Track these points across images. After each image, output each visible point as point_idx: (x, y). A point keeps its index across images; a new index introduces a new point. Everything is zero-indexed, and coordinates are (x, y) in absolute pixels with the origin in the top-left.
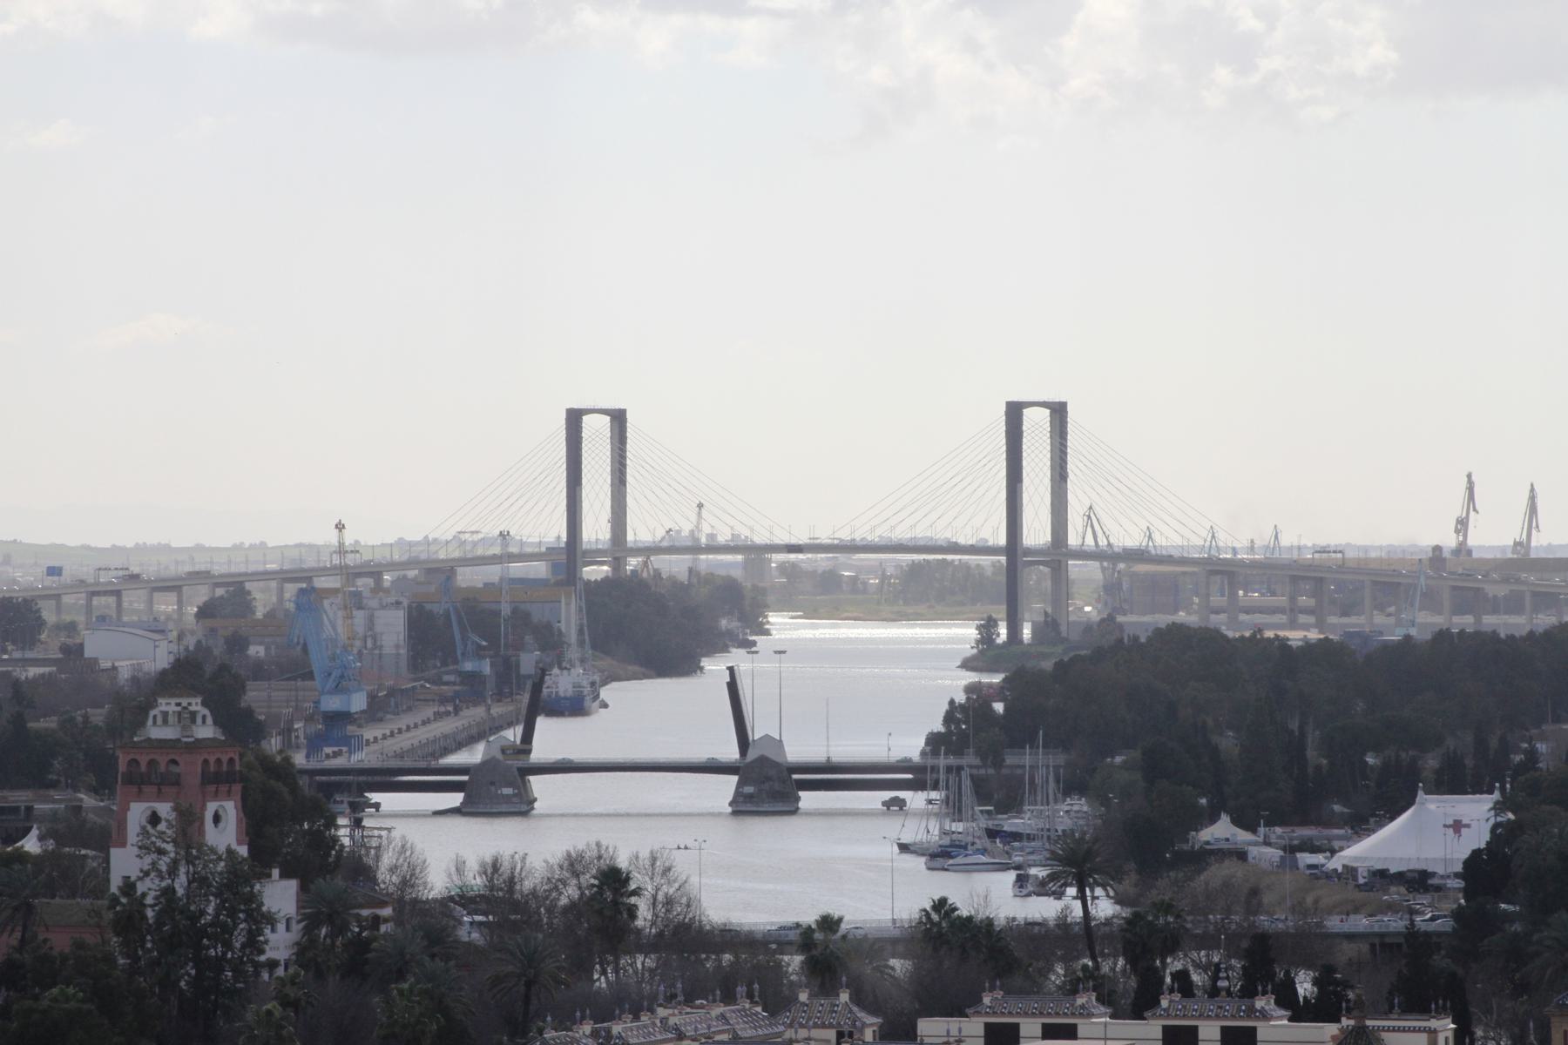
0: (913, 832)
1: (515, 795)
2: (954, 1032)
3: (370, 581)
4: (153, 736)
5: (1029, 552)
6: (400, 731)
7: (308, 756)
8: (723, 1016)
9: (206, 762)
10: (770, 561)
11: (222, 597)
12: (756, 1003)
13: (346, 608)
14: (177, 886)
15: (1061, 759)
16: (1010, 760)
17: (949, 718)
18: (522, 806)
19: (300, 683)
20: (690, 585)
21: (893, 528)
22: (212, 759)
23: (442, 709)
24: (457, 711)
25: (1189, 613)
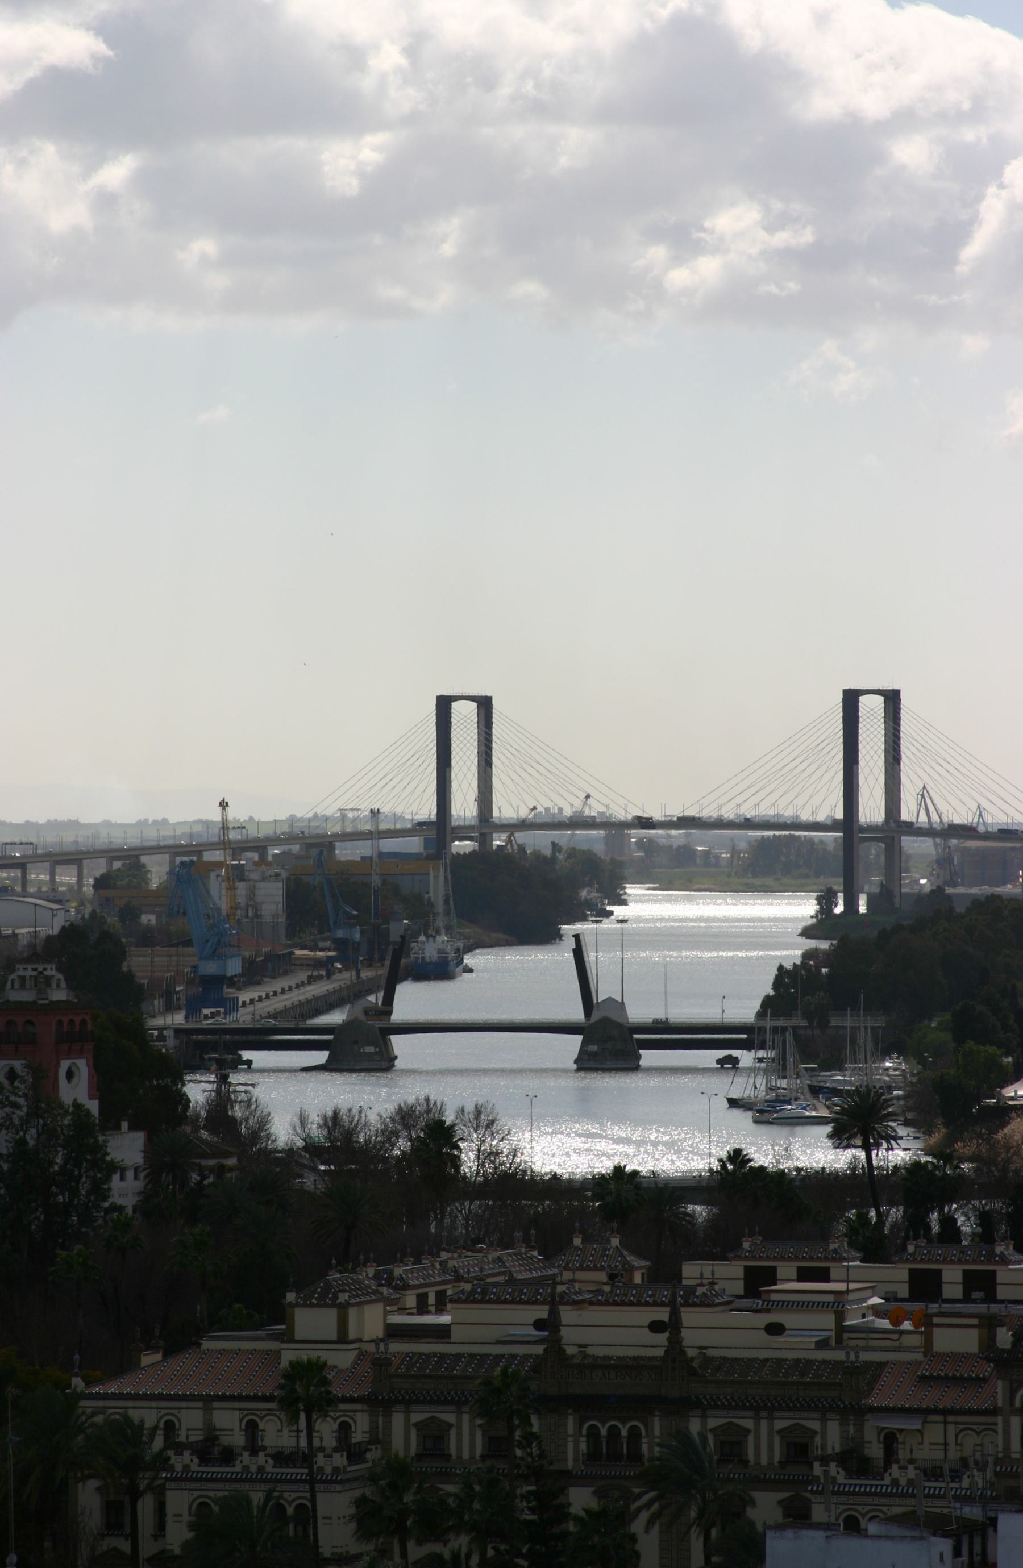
0: (741, 1087)
1: (376, 1053)
2: (707, 1274)
3: (256, 857)
4: (11, 999)
5: (863, 829)
6: (275, 994)
7: (186, 1018)
8: (499, 1259)
9: (60, 1022)
10: (629, 836)
11: (119, 870)
12: (533, 1248)
13: (228, 879)
14: (28, 1137)
15: (880, 1022)
16: (834, 1023)
17: (777, 984)
18: (383, 1062)
19: (181, 949)
20: (554, 858)
21: (720, 807)
22: (65, 1020)
23: (315, 973)
24: (329, 976)
25: (1015, 886)
